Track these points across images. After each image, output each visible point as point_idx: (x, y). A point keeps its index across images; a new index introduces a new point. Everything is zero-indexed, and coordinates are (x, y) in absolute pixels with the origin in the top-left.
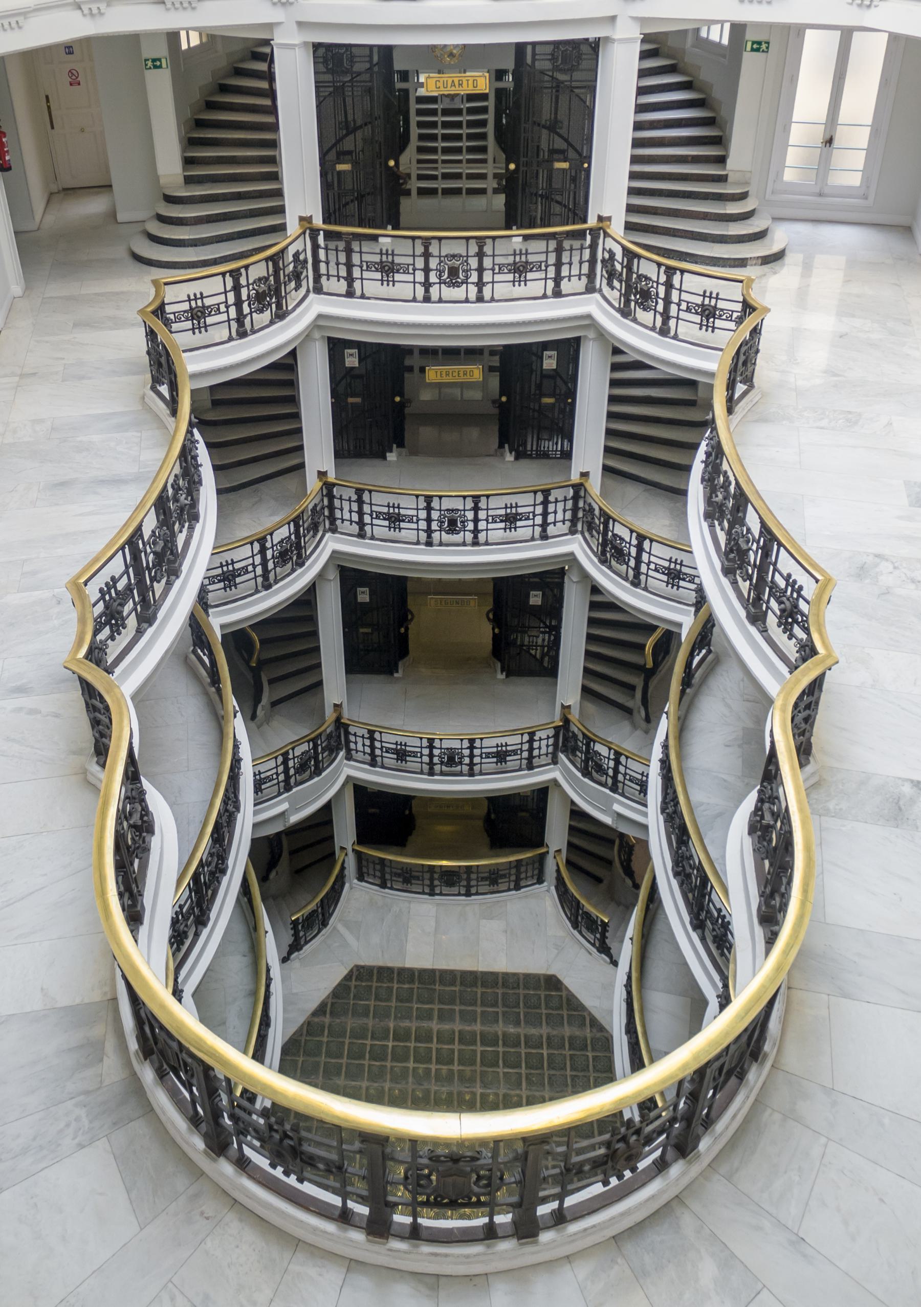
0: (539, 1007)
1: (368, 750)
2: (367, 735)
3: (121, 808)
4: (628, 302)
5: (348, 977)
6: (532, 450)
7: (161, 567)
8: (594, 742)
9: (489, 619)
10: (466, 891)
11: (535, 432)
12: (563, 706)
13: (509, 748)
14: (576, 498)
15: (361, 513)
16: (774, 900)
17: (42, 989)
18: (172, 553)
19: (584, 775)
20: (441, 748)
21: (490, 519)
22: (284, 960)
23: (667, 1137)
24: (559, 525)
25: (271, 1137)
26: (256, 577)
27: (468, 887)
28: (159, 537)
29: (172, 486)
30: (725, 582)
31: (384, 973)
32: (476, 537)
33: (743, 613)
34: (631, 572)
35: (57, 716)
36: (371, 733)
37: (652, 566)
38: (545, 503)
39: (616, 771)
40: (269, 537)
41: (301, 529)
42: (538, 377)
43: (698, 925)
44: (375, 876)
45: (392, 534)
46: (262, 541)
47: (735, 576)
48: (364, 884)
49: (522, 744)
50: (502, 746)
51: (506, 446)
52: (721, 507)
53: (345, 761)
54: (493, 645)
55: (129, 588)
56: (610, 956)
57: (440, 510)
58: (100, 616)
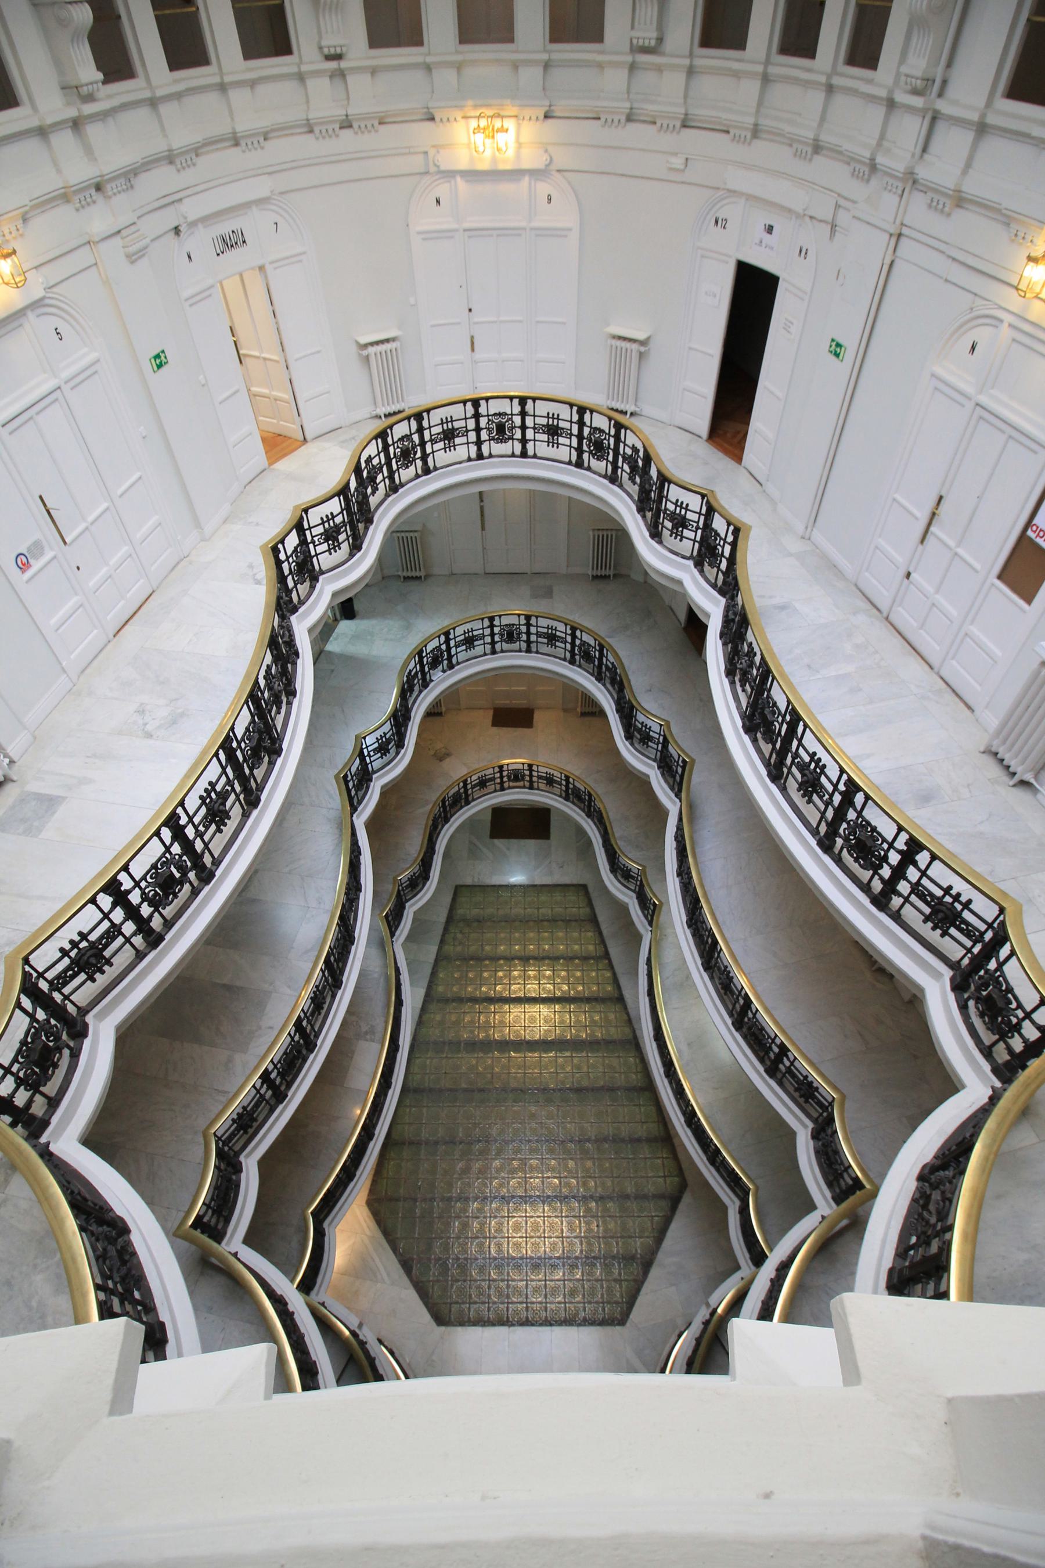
40: (280, 546)
57: (501, 626)
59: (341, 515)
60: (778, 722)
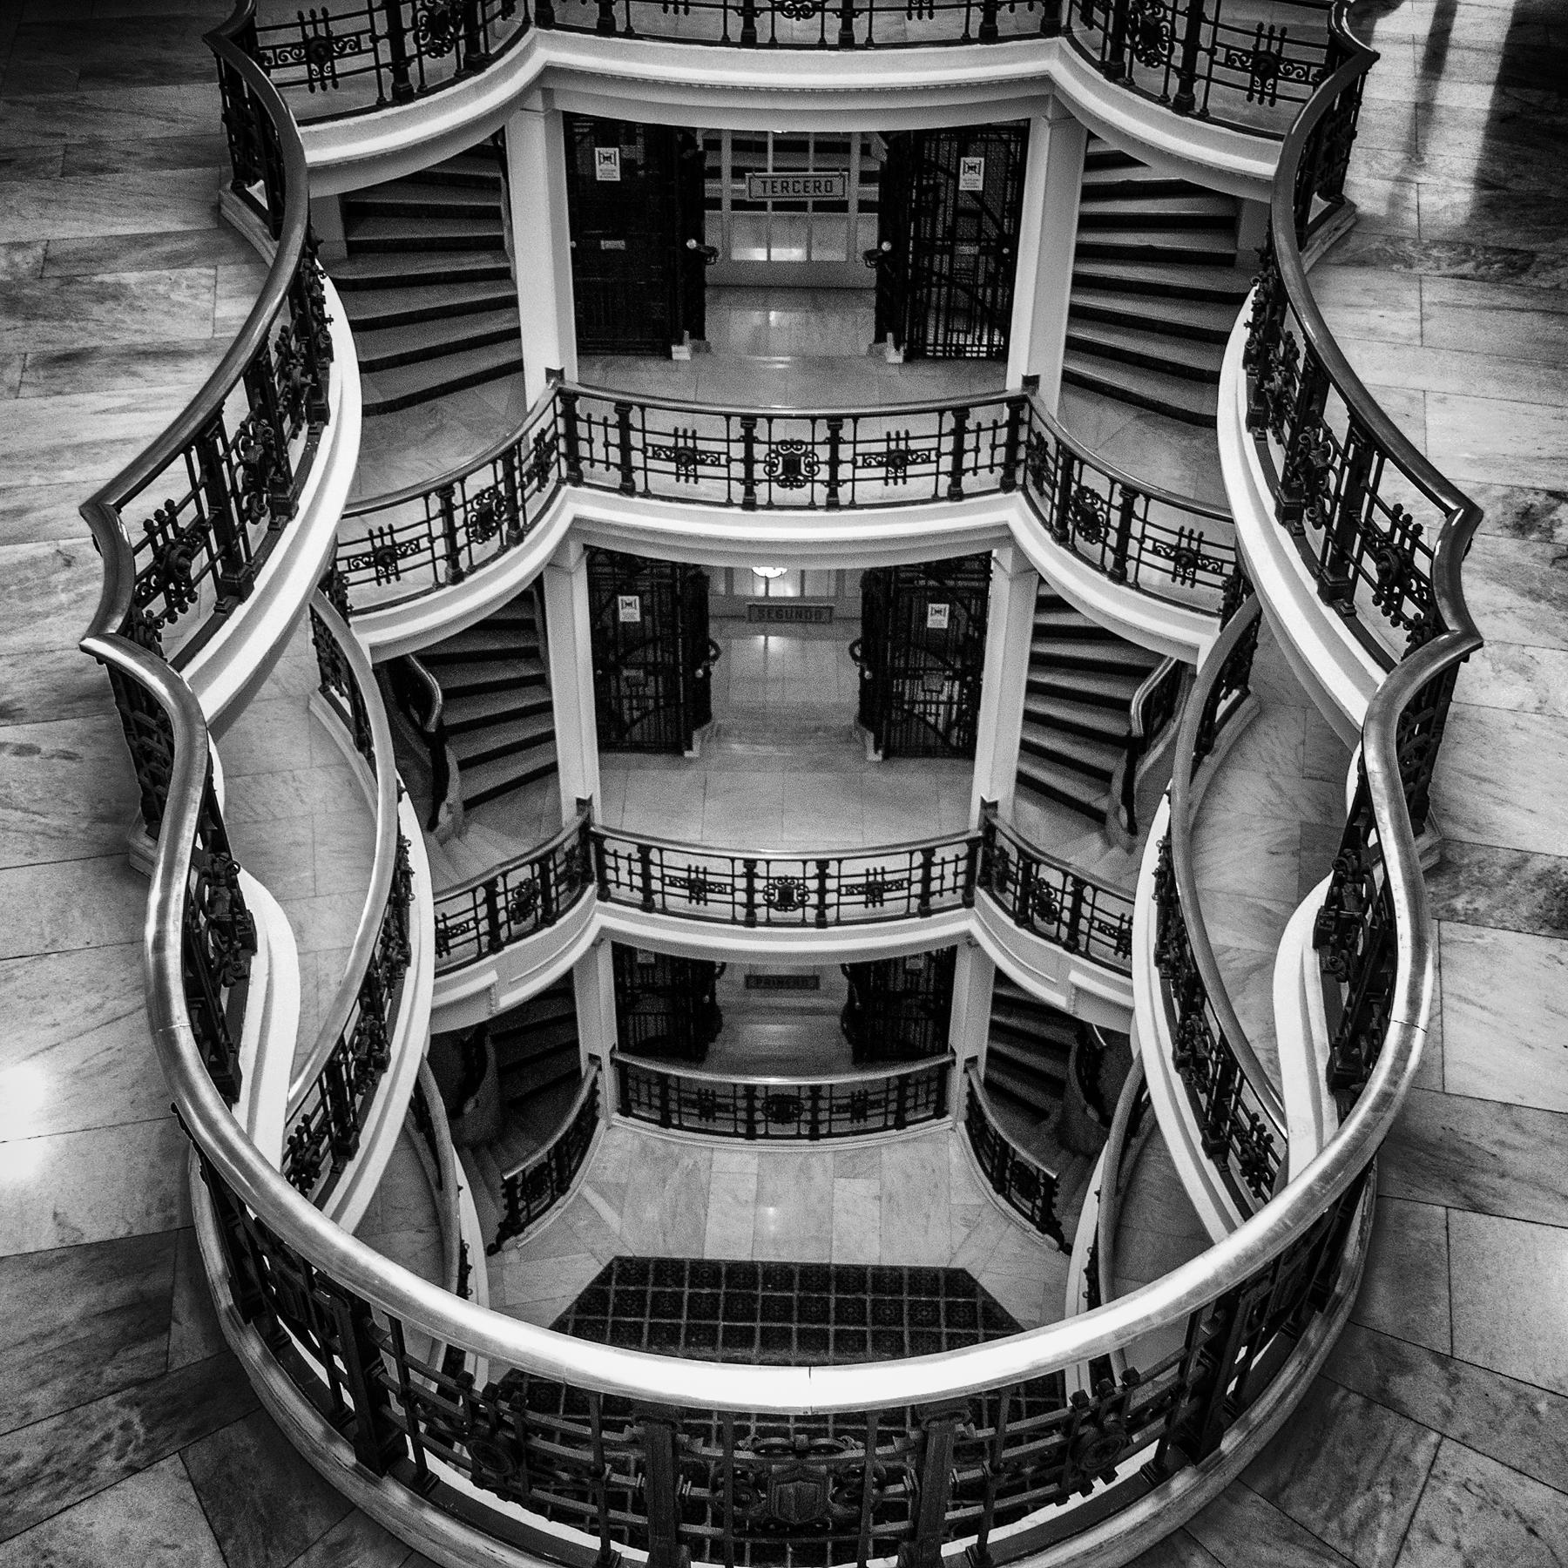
0: (936, 1323)
1: (638, 881)
2: (636, 856)
3: (193, 890)
4: (1117, 53)
5: (604, 1278)
6: (936, 344)
7: (260, 493)
8: (1039, 863)
9: (854, 657)
10: (811, 1130)
11: (942, 318)
12: (985, 805)
13: (888, 877)
14: (1014, 424)
15: (625, 448)
16: (1359, 1046)
17: (56, 1215)
18: (279, 470)
19: (1019, 923)
20: (768, 878)
21: (860, 459)
22: (492, 1250)
23: (1167, 1422)
24: (983, 473)
25: (475, 1426)
26: (434, 560)
27: (814, 1125)
28: (255, 437)
29: (277, 347)
30: (1283, 534)
31: (668, 1269)
32: (833, 493)
33: (1312, 586)
34: (1110, 557)
35: (69, 756)
36: (644, 850)
37: (1149, 544)
38: (959, 432)
39: (1076, 912)
40: (457, 486)
41: (517, 474)
42: (950, 211)
43: (1216, 1149)
44: (650, 1106)
45: (683, 488)
46: (445, 491)
47: (1300, 522)
48: (631, 1120)
49: (911, 869)
50: (876, 873)
51: (890, 335)
52: (1279, 398)
53: (598, 902)
54: (862, 703)
55: (199, 526)
56: (1059, 1237)
58: (147, 573)
59: (192, 504)
60: (1334, 470)
